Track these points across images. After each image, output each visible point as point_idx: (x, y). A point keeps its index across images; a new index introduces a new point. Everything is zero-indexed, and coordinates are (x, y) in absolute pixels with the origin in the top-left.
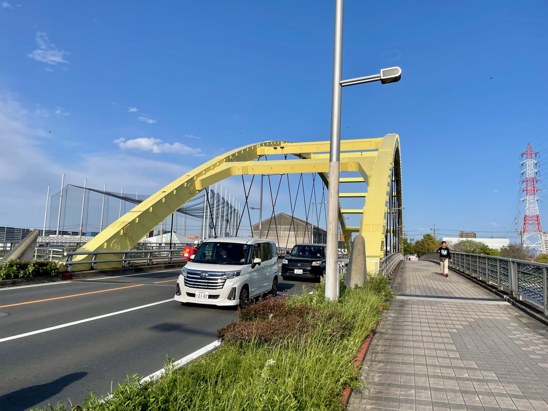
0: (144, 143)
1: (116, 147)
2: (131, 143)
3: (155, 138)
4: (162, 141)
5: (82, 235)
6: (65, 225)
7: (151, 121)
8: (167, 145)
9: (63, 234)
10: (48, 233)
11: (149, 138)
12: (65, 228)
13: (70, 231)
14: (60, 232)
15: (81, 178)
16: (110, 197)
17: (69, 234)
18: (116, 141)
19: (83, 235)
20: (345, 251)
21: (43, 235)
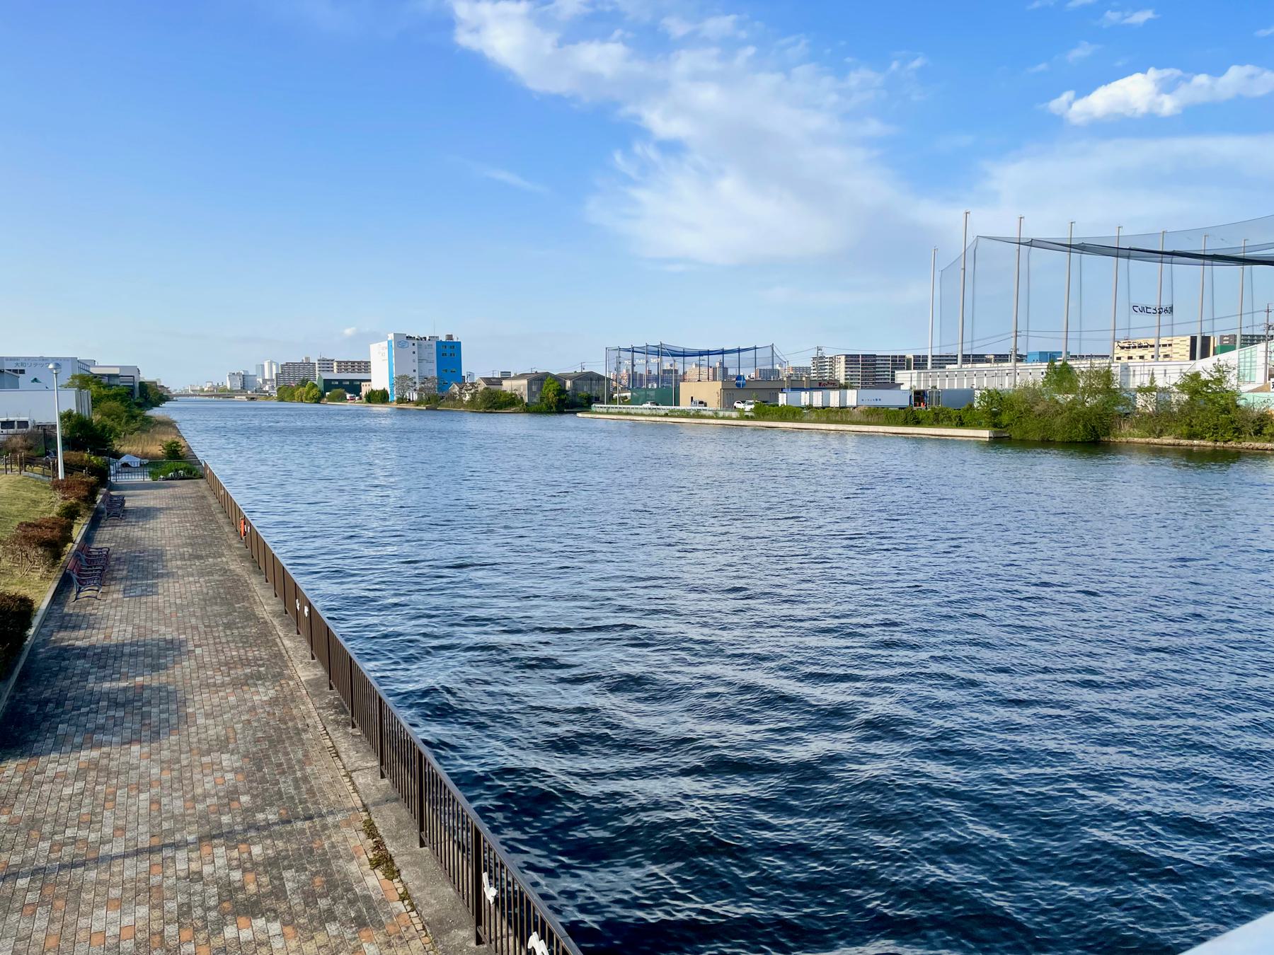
0: (1135, 91)
1: (1058, 121)
2: (1102, 100)
3: (1159, 67)
4: (1178, 72)
5: (1018, 361)
6: (1154, 303)
7: (1141, 17)
8: (1202, 79)
9: (974, 362)
10: (942, 361)
11: (1144, 72)
12: (976, 344)
13: (989, 352)
14: (964, 356)
15: (994, 220)
16: (1088, 258)
17: (988, 361)
18: (1057, 105)
19: (1021, 361)
20: (189, 833)
21: (929, 366)
